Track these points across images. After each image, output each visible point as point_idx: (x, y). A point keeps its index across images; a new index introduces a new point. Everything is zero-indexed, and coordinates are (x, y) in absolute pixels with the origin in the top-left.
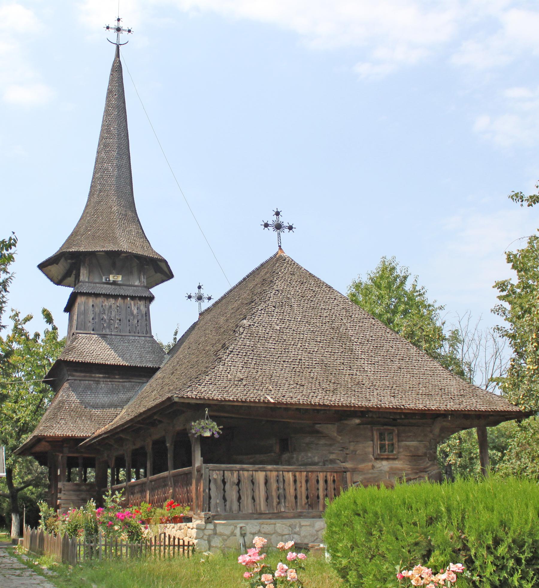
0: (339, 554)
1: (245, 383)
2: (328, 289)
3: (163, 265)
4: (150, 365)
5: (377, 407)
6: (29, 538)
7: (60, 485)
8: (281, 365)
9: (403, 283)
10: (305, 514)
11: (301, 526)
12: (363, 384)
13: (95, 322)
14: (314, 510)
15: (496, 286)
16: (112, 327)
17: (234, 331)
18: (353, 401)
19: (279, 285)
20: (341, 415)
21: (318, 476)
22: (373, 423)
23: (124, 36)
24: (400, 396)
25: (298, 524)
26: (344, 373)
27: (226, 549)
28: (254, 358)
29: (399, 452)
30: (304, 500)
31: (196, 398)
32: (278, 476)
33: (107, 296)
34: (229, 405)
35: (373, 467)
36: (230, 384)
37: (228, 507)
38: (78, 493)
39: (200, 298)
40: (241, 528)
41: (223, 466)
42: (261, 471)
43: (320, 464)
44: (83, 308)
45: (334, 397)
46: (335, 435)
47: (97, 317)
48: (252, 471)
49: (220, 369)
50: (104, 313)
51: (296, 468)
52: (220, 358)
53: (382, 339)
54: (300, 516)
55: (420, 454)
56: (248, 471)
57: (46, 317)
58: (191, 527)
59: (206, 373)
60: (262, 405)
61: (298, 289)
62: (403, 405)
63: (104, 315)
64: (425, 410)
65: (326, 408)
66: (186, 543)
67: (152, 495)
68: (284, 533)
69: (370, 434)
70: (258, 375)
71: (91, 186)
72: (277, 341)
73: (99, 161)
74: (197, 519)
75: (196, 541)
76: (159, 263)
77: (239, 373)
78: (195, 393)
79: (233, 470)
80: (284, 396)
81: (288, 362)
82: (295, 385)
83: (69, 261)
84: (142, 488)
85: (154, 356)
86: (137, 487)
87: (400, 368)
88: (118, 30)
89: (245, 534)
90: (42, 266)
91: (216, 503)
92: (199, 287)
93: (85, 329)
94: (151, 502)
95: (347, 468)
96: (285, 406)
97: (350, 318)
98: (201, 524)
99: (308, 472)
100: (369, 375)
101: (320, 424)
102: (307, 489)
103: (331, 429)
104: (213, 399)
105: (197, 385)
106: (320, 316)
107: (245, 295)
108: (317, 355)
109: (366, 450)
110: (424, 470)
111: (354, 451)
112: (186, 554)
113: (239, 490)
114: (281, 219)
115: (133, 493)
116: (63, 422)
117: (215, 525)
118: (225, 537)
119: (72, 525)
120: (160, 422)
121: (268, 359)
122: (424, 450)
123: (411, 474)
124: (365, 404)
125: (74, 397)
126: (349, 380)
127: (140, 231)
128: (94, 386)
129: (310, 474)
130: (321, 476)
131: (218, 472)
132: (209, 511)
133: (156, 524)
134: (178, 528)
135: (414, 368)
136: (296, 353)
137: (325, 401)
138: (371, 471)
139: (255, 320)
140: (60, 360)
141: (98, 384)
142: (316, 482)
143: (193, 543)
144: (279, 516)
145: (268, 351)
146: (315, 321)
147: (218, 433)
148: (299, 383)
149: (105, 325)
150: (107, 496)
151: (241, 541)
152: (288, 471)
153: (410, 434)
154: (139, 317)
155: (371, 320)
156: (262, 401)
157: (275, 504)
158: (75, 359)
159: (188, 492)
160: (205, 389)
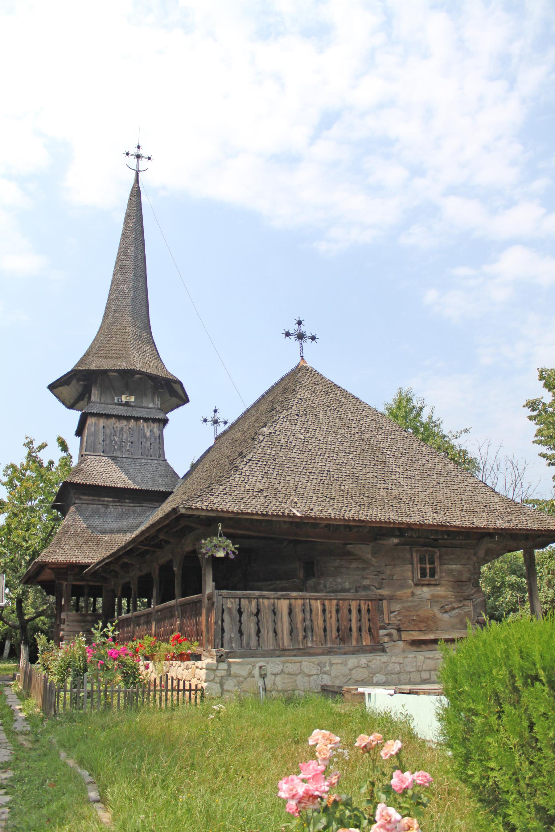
0: (492, 764)
1: (265, 494)
2: (356, 400)
3: (176, 387)
4: (162, 489)
5: (420, 523)
6: (23, 674)
7: (63, 615)
8: (306, 477)
9: (418, 414)
10: (335, 649)
11: (331, 665)
12: (401, 499)
13: (106, 444)
14: (346, 645)
15: (527, 405)
16: (124, 450)
17: (253, 439)
18: (392, 517)
19: (302, 393)
20: (376, 533)
21: (350, 605)
22: (412, 545)
23: (144, 164)
24: (443, 513)
26: (378, 487)
27: (242, 694)
28: (276, 468)
29: (441, 577)
30: (335, 634)
31: (207, 510)
32: (304, 605)
33: (119, 417)
34: (247, 519)
35: (413, 594)
36: (249, 496)
37: (244, 642)
38: (83, 624)
39: (216, 422)
40: (260, 667)
41: (239, 592)
42: (284, 599)
43: (352, 591)
44: (93, 429)
45: (370, 511)
46: (370, 556)
47: (107, 439)
48: (274, 598)
49: (236, 479)
50: (116, 435)
51: (324, 596)
52: (236, 467)
53: (417, 452)
54: (329, 652)
55: (464, 580)
56: (268, 598)
57: (61, 446)
58: (200, 667)
59: (220, 483)
60: (287, 519)
61: (322, 398)
62: (449, 522)
63: (115, 437)
64: (473, 528)
65: (361, 524)
66: (193, 687)
67: (158, 627)
68: (312, 673)
69: (408, 556)
70: (281, 487)
71: (107, 308)
72: (302, 451)
73: (115, 282)
74: (207, 657)
75: (206, 684)
76: (173, 385)
77: (258, 483)
78: (205, 504)
79: (251, 598)
80: (312, 510)
81: (314, 473)
82: (324, 498)
83: (81, 383)
84: (148, 619)
85: (166, 480)
86: (143, 618)
87: (439, 483)
88: (138, 156)
89: (265, 674)
90: (52, 387)
91: (231, 637)
92: (215, 411)
93: (94, 451)
94: (157, 635)
95: (383, 595)
96: (313, 521)
97: (380, 430)
98: (212, 664)
99: (339, 600)
100: (406, 489)
101: (351, 544)
102: (338, 621)
103: (364, 551)
104: (228, 512)
105: (208, 496)
106: (348, 427)
107: (264, 407)
108: (347, 467)
109: (405, 574)
110: (468, 598)
112: (193, 701)
113: (259, 621)
114: (303, 329)
115: (138, 625)
116: (67, 547)
117: (229, 664)
118: (241, 679)
119: (65, 661)
120: (167, 542)
121: (292, 469)
122: (469, 576)
124: (405, 520)
125: (80, 522)
126: (385, 495)
127: (155, 352)
128: (102, 510)
129: (341, 602)
131: (233, 600)
132: (222, 646)
133: (160, 661)
134: (185, 667)
135: (453, 483)
136: (323, 464)
137: (360, 516)
138: (410, 599)
139: (276, 428)
140: (67, 482)
141: (106, 508)
142: (348, 612)
143: (202, 687)
144: (305, 652)
145: (291, 461)
146: (343, 431)
147: (233, 552)
148: (329, 496)
149: (116, 447)
150: (96, 629)
151: (261, 683)
152: (316, 599)
153: (452, 557)
154: (153, 440)
155: (403, 432)
156: (286, 514)
157: (300, 638)
158: (83, 481)
159: (198, 624)
160: (219, 500)
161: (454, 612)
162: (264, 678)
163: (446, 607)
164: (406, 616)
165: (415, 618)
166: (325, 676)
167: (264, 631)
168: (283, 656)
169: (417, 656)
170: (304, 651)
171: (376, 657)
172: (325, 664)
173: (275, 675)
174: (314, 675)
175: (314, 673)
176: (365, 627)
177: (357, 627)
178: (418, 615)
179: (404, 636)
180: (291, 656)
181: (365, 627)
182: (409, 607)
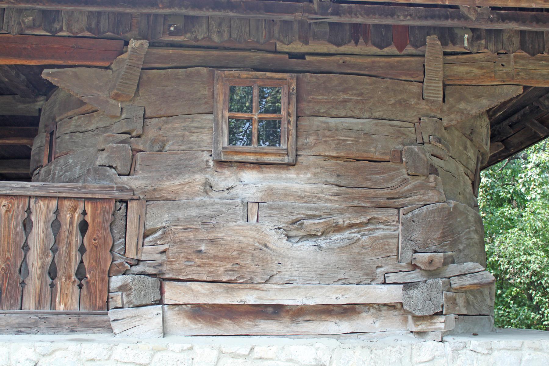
21: (29, 211)
35: (208, 187)
50: (541, 283)
109: (193, 138)
110: (391, 203)
123: (341, 211)
130: (41, 212)
153: (343, 96)
161: (338, 236)
163: (307, 223)
164: (183, 242)
165: (203, 247)
169: (196, 348)
177: (43, 267)
178: (212, 241)
179: (173, 293)
182: (191, 220)
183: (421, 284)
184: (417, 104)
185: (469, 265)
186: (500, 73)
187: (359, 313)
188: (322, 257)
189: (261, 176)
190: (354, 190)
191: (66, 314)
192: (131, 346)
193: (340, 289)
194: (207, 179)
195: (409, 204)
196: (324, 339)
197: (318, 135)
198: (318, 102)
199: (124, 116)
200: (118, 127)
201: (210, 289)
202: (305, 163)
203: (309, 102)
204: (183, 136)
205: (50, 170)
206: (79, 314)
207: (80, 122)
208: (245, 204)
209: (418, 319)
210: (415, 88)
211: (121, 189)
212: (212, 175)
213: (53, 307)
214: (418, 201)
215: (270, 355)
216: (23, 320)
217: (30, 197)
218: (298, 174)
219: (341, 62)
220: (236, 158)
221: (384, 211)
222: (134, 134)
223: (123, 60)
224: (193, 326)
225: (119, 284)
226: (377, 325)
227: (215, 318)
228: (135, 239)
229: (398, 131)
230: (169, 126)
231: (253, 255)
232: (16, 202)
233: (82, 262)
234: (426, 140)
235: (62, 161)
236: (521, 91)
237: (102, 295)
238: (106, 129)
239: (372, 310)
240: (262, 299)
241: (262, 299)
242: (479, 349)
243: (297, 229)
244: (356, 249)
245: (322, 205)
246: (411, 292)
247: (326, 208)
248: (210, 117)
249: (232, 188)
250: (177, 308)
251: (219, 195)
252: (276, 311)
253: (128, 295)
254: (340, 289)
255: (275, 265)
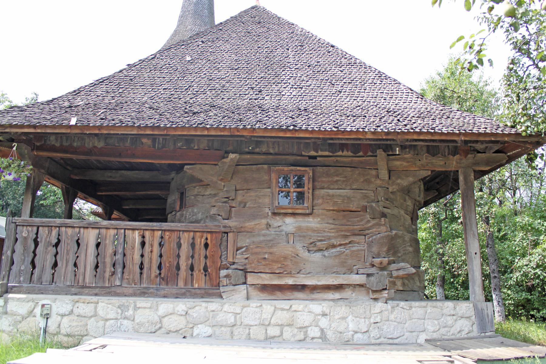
10: (152, 290)
14: (170, 286)
21: (179, 238)
25: (132, 305)
35: (268, 226)
37: (35, 276)
40: (43, 306)
42: (93, 228)
79: (52, 226)
102: (161, 256)
110: (361, 233)
111: (244, 204)
113: (57, 253)
118: (18, 317)
123: (335, 237)
129: (167, 233)
130: (185, 239)
151: (42, 325)
152: (133, 230)
153: (336, 178)
157: (107, 274)
161: (334, 250)
162: (47, 318)
163: (318, 243)
164: (256, 253)
165: (266, 256)
166: (125, 322)
167: (62, 265)
168: (81, 295)
169: (264, 306)
170: (108, 290)
171: (201, 303)
172: (128, 307)
173: (63, 316)
174: (112, 319)
175: (112, 317)
176: (200, 265)
177: (187, 265)
178: (271, 253)
180: (91, 295)
181: (200, 265)
182: (261, 242)
183: (376, 275)
184: (375, 181)
185: (402, 264)
186: (418, 164)
187: (344, 289)
188: (326, 261)
189: (295, 220)
190: (342, 226)
191: (199, 289)
192: (232, 304)
193: (334, 277)
194: (268, 222)
195: (371, 233)
196: (327, 302)
197: (323, 199)
198: (323, 182)
199: (225, 189)
200: (221, 194)
201: (270, 277)
202: (317, 213)
203: (319, 182)
204: (255, 200)
205: (183, 214)
206: (205, 289)
207: (200, 190)
208: (287, 235)
209: (374, 291)
210: (374, 172)
211: (225, 227)
212: (270, 220)
213: (192, 285)
214: (375, 231)
215: (300, 309)
216: (178, 292)
217: (180, 231)
218: (313, 219)
219: (335, 160)
220: (282, 211)
221: (358, 237)
222: (231, 198)
223: (226, 163)
224: (262, 295)
225: (225, 274)
226: (354, 295)
227: (273, 291)
228: (232, 252)
229: (365, 196)
230: (248, 194)
231: (291, 260)
232: (173, 233)
233: (206, 263)
234: (380, 199)
235: (190, 210)
236: (430, 173)
237: (216, 280)
238: (215, 195)
239: (351, 287)
240: (296, 281)
241: (296, 281)
242: (405, 307)
243: (313, 247)
244: (343, 257)
245: (326, 234)
246: (370, 278)
247: (327, 236)
248: (269, 190)
249: (280, 226)
250: (253, 286)
251: (274, 230)
252: (303, 288)
253: (230, 280)
254: (334, 277)
255: (302, 265)
